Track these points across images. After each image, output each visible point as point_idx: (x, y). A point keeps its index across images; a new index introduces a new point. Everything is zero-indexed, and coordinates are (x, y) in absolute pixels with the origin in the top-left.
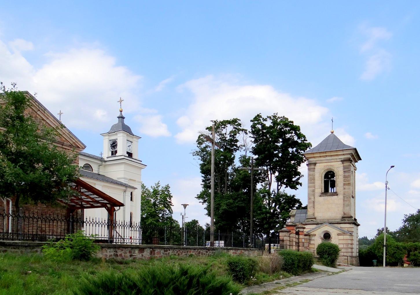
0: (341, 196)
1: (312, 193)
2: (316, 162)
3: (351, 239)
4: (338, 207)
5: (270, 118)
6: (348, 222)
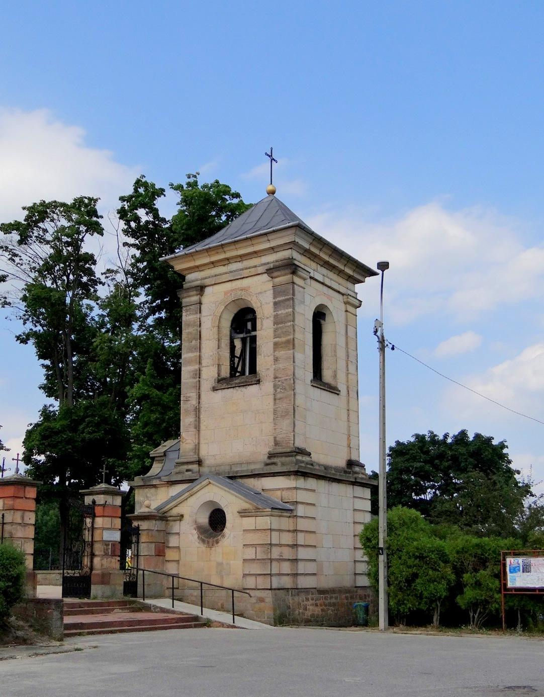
0: (267, 386)
1: (191, 380)
2: (203, 281)
3: (291, 529)
4: (261, 422)
5: (179, 188)
6: (284, 469)
